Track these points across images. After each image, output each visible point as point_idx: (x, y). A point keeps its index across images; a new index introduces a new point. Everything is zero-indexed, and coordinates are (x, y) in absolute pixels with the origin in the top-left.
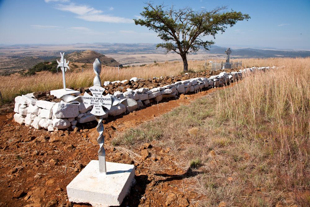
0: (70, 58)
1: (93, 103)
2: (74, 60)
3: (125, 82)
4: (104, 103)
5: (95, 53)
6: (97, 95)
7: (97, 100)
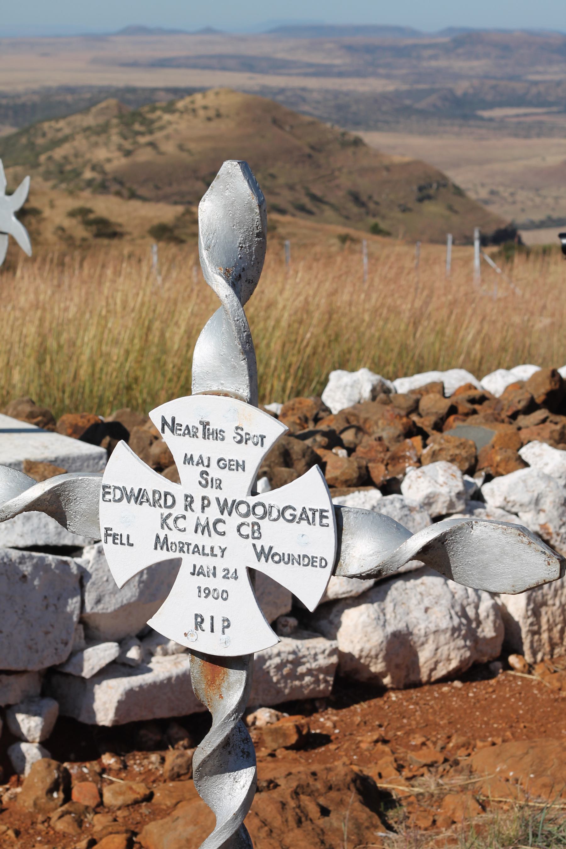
0: (58, 153)
1: (174, 537)
2: (88, 174)
3: (519, 385)
4: (265, 542)
5: (275, 122)
6: (214, 472)
7: (213, 513)
